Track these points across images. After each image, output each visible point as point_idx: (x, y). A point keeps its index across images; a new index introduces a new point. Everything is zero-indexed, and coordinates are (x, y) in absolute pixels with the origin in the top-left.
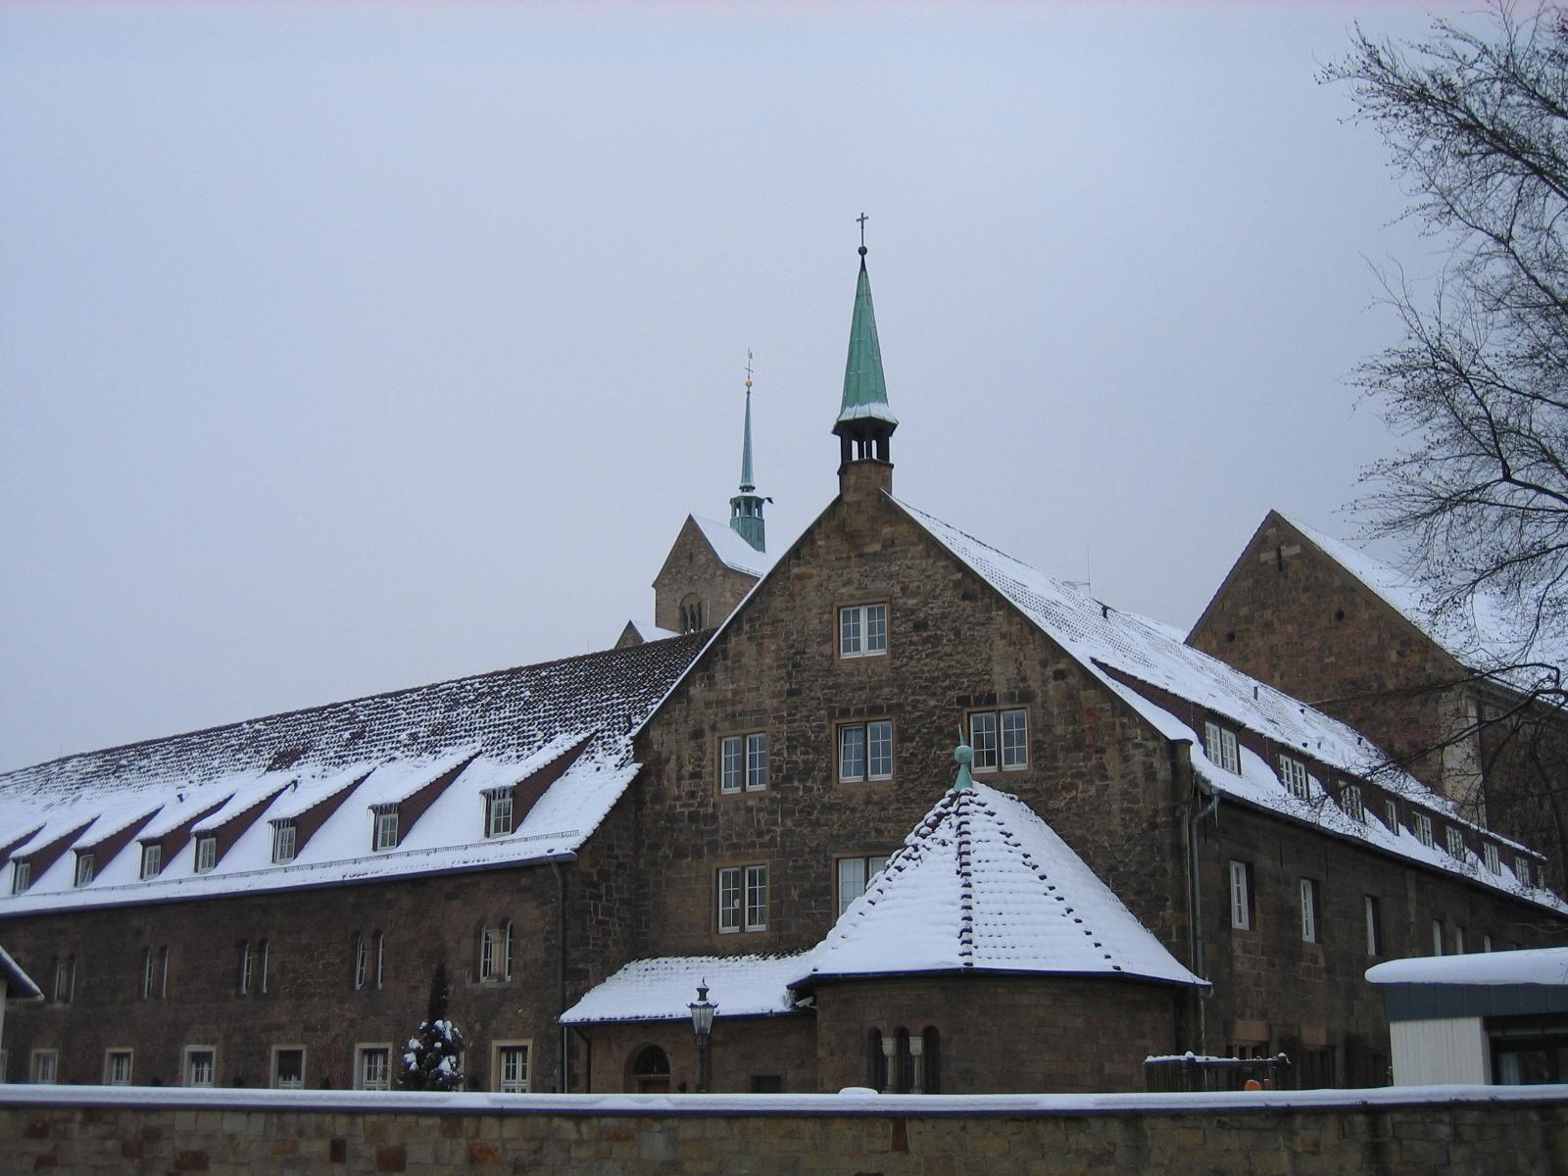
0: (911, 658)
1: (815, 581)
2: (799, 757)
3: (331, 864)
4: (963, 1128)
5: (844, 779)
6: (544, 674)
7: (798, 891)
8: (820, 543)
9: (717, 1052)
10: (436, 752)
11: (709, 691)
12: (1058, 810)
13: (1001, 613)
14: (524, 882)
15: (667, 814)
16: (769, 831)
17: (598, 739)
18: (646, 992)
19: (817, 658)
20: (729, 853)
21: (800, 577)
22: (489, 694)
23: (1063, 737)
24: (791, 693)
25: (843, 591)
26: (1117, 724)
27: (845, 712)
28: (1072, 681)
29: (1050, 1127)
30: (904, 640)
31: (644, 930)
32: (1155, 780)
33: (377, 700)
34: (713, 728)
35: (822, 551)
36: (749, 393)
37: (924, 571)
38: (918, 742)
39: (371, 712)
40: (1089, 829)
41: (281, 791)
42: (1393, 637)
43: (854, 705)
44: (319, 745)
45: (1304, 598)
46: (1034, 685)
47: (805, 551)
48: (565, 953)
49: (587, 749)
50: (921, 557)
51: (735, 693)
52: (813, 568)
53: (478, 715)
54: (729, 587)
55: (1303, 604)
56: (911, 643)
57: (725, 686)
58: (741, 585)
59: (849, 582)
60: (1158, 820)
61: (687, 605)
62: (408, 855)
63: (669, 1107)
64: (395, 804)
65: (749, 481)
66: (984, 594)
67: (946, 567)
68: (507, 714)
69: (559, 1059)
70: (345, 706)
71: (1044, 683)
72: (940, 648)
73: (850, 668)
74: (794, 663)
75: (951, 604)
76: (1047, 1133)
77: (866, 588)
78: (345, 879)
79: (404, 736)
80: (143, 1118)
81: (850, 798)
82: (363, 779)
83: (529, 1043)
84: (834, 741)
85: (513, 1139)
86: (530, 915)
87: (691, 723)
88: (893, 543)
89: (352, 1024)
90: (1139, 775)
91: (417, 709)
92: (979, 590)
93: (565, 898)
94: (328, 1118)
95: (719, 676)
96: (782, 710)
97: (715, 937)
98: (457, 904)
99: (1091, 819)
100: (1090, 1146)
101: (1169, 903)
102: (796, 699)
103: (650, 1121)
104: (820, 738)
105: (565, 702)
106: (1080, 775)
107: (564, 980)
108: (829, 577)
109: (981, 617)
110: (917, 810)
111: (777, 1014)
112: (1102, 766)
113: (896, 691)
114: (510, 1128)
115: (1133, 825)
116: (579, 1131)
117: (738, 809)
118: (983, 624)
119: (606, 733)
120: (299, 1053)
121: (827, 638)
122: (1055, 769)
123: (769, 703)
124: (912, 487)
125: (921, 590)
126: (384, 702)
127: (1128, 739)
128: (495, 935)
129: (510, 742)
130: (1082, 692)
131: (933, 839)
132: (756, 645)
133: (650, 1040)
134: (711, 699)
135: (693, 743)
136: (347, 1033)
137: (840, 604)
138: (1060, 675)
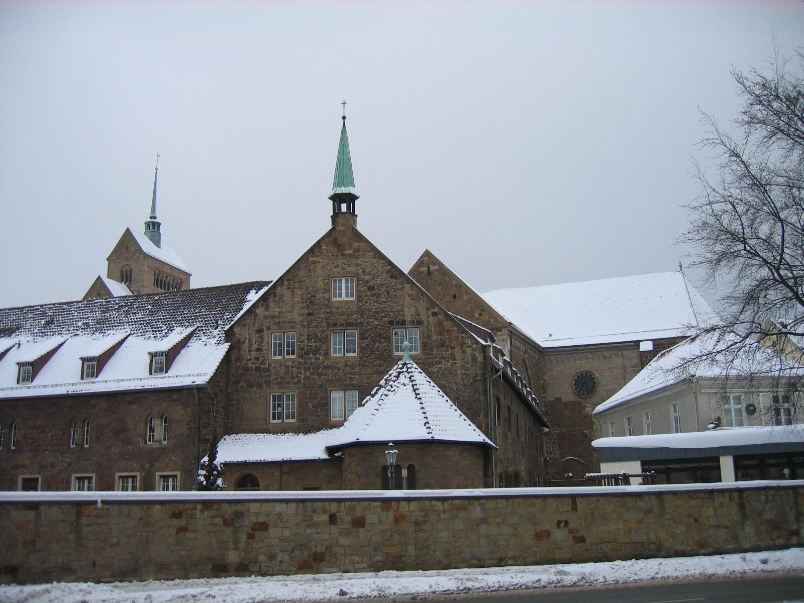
0: (367, 302)
1: (321, 264)
2: (312, 344)
3: (57, 385)
4: (598, 500)
5: (334, 355)
6: (156, 298)
7: (312, 405)
8: (323, 247)
10: (103, 333)
11: (266, 311)
12: (433, 372)
13: (408, 285)
14: (175, 397)
15: (244, 367)
16: (297, 377)
17: (199, 330)
18: (234, 449)
19: (322, 299)
21: (314, 262)
22: (126, 306)
23: (436, 341)
24: (309, 314)
25: (335, 270)
26: (460, 337)
27: (335, 325)
28: (440, 317)
29: (630, 499)
30: (363, 294)
32: (476, 361)
33: (56, 305)
34: (268, 328)
35: (324, 251)
36: (156, 173)
37: (373, 264)
38: (369, 340)
39: (54, 311)
40: (447, 381)
41: (11, 348)
42: (477, 307)
43: (340, 321)
44: (26, 326)
45: (439, 288)
46: (423, 318)
47: (316, 251)
48: (199, 431)
49: (195, 335)
50: (372, 258)
51: (280, 313)
52: (320, 258)
53: (123, 316)
54: (146, 263)
55: (438, 291)
56: (367, 296)
57: (274, 309)
58: (152, 263)
59: (337, 266)
60: (477, 378)
61: (124, 270)
62: (106, 382)
63: (482, 494)
64: (96, 357)
65: (155, 214)
66: (400, 276)
67: (383, 263)
68: (140, 316)
70: (37, 307)
71: (428, 317)
72: (380, 299)
73: (337, 305)
74: (310, 301)
75: (385, 280)
76: (630, 502)
77: (345, 269)
78: (69, 393)
79: (80, 324)
80: (233, 507)
81: (337, 363)
82: (62, 344)
83: (178, 473)
84: (329, 336)
85: (415, 511)
86: (178, 412)
87: (256, 325)
88: (359, 250)
89: (70, 464)
90: (469, 359)
91: (83, 311)
92: (399, 274)
94: (327, 504)
95: (272, 305)
96: (305, 322)
98: (135, 406)
99: (448, 376)
100: (644, 506)
101: (482, 414)
102: (312, 318)
103: (473, 501)
104: (323, 336)
105: (174, 312)
106: (443, 358)
107: (199, 444)
108: (328, 263)
109: (400, 287)
110: (369, 370)
112: (453, 354)
113: (359, 316)
114: (413, 506)
115: (466, 380)
116: (443, 506)
117: (281, 366)
118: (400, 290)
119: (203, 328)
120: (37, 479)
121: (327, 291)
122: (433, 355)
123: (299, 319)
124: (366, 224)
125: (372, 272)
126: (60, 307)
127: (465, 343)
129: (147, 330)
130: (444, 322)
131: (399, 383)
132: (291, 292)
133: (248, 472)
134: (267, 315)
135: (257, 335)
136: (67, 469)
137: (333, 276)
138: (434, 314)
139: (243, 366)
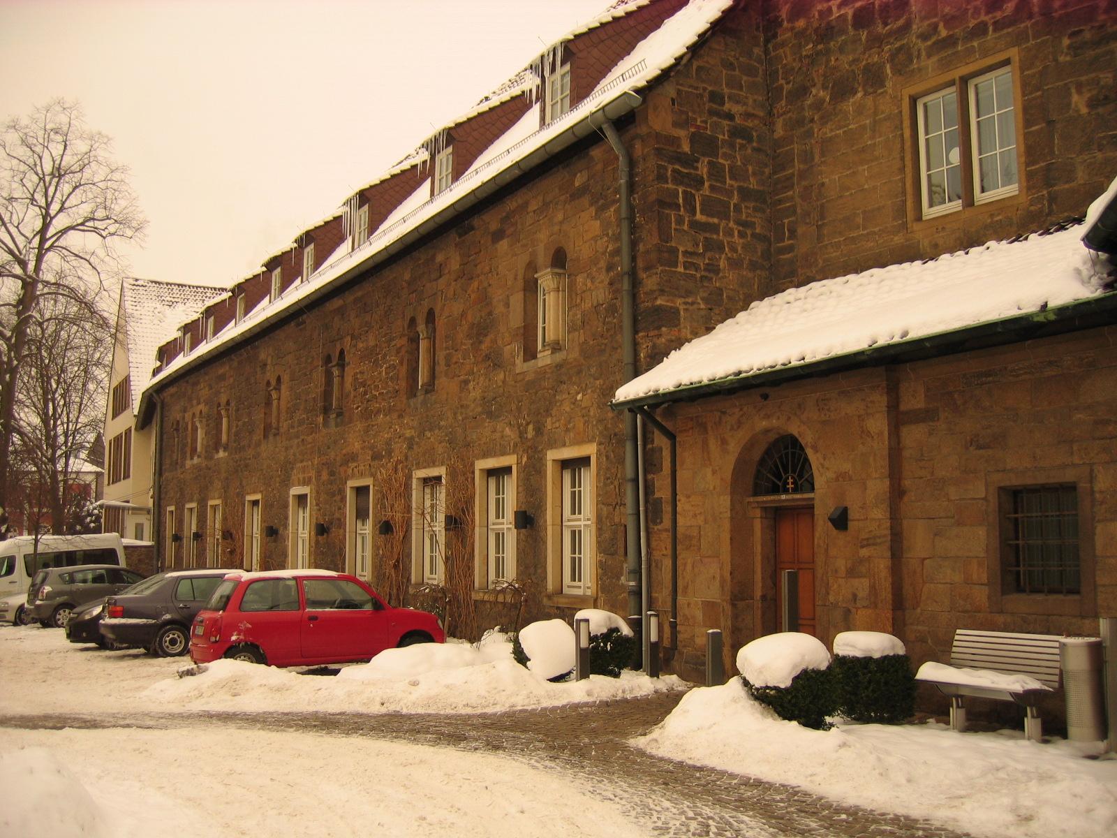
9: (913, 435)
15: (816, 30)
20: (935, 59)
31: (787, 242)
48: (635, 283)
69: (629, 473)
93: (631, 187)
97: (917, 227)
98: (503, 245)
111: (1062, 310)
128: (546, 280)
133: (774, 422)
139: (815, 25)
